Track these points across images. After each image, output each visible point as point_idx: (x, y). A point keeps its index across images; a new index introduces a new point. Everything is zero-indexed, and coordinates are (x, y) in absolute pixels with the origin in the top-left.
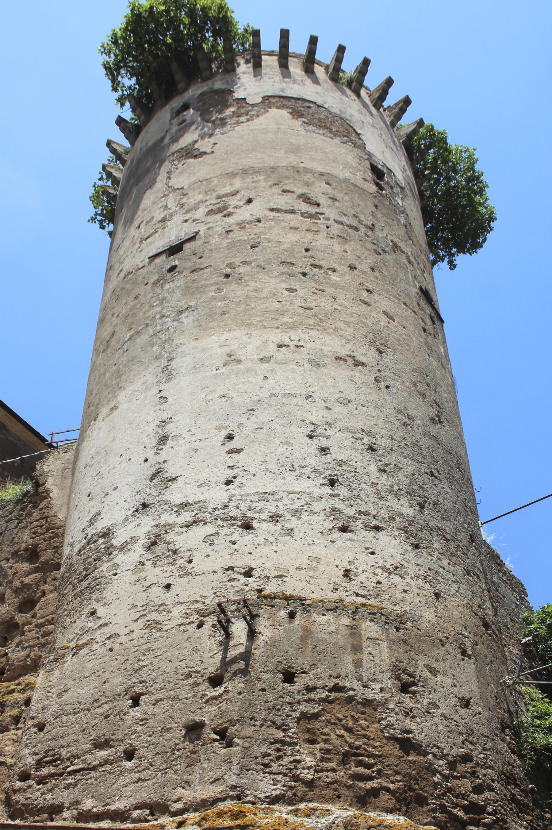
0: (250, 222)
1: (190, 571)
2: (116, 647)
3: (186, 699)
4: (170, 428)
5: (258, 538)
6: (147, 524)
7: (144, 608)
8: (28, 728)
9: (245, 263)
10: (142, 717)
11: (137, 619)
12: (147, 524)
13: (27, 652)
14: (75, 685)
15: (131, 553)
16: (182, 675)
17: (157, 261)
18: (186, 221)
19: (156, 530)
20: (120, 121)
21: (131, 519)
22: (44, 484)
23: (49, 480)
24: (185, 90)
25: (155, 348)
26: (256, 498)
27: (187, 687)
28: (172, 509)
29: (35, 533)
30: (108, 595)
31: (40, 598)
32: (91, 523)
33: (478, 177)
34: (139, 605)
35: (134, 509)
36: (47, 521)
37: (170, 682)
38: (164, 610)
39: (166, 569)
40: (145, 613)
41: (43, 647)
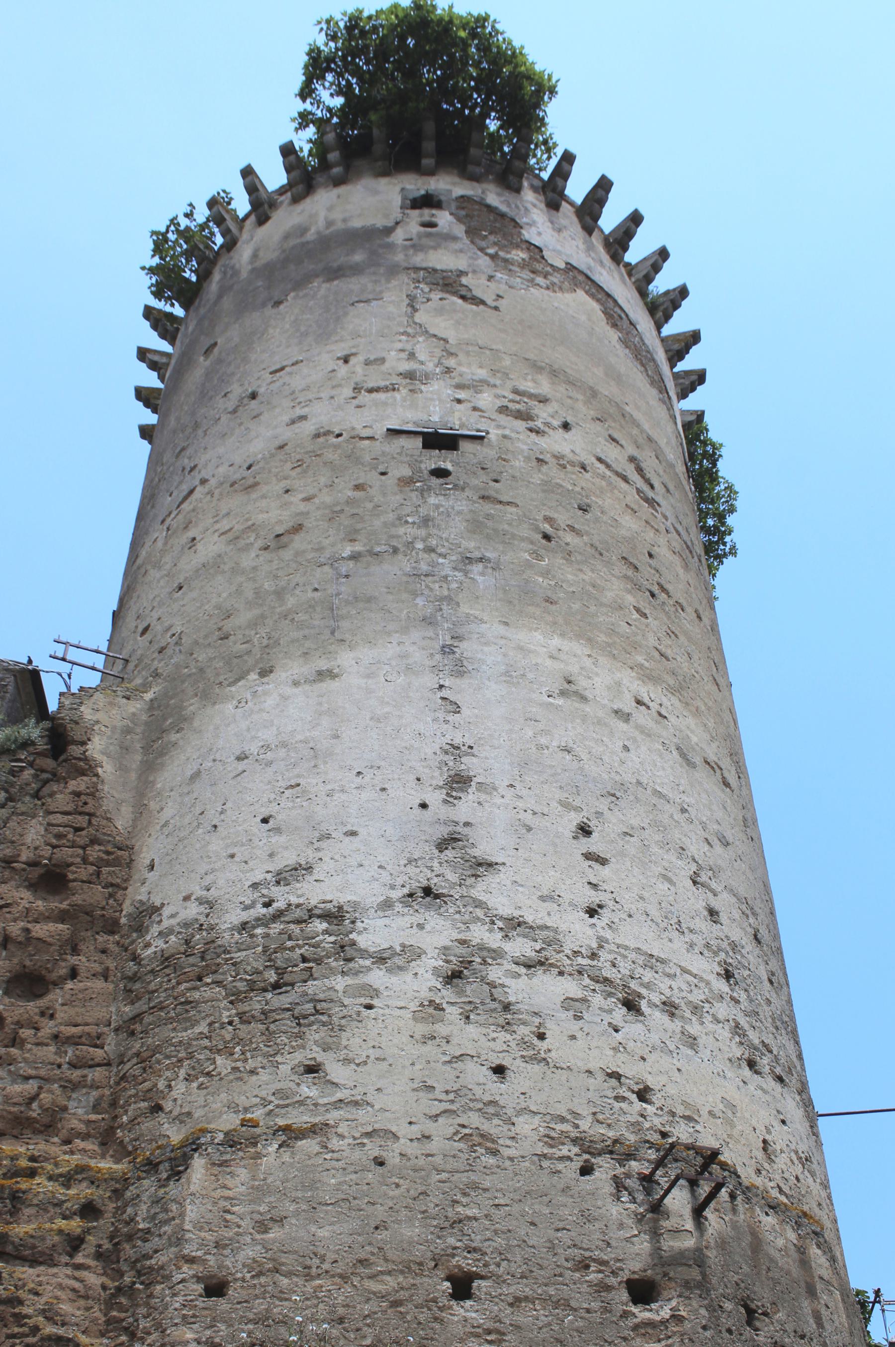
0: (573, 464)
1: (543, 1055)
2: (393, 1159)
3: (588, 1311)
4: (470, 765)
5: (652, 1035)
6: (437, 933)
7: (451, 1096)
8: (183, 1281)
9: (572, 528)
10: (489, 1325)
11: (437, 1116)
12: (437, 933)
13: (31, 1086)
14: (297, 1213)
15: (408, 977)
16: (567, 1260)
17: (403, 441)
18: (459, 401)
19: (462, 950)
20: (288, 150)
21: (399, 907)
22: (83, 743)
23: (96, 739)
24: (431, 173)
25: (420, 601)
26: (641, 960)
27: (584, 1288)
28: (493, 923)
29: (59, 836)
30: (354, 1041)
31: (63, 980)
32: (281, 879)
33: (724, 533)
34: (440, 1088)
35: (406, 891)
36: (90, 822)
37: (541, 1267)
38: (497, 1115)
39: (495, 1035)
40: (453, 1107)
41: (73, 1090)
